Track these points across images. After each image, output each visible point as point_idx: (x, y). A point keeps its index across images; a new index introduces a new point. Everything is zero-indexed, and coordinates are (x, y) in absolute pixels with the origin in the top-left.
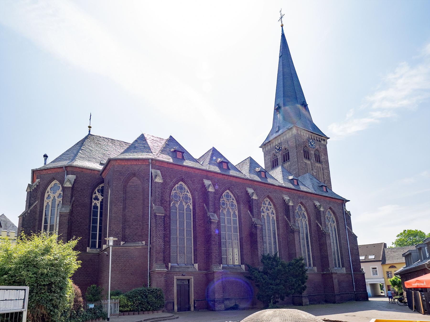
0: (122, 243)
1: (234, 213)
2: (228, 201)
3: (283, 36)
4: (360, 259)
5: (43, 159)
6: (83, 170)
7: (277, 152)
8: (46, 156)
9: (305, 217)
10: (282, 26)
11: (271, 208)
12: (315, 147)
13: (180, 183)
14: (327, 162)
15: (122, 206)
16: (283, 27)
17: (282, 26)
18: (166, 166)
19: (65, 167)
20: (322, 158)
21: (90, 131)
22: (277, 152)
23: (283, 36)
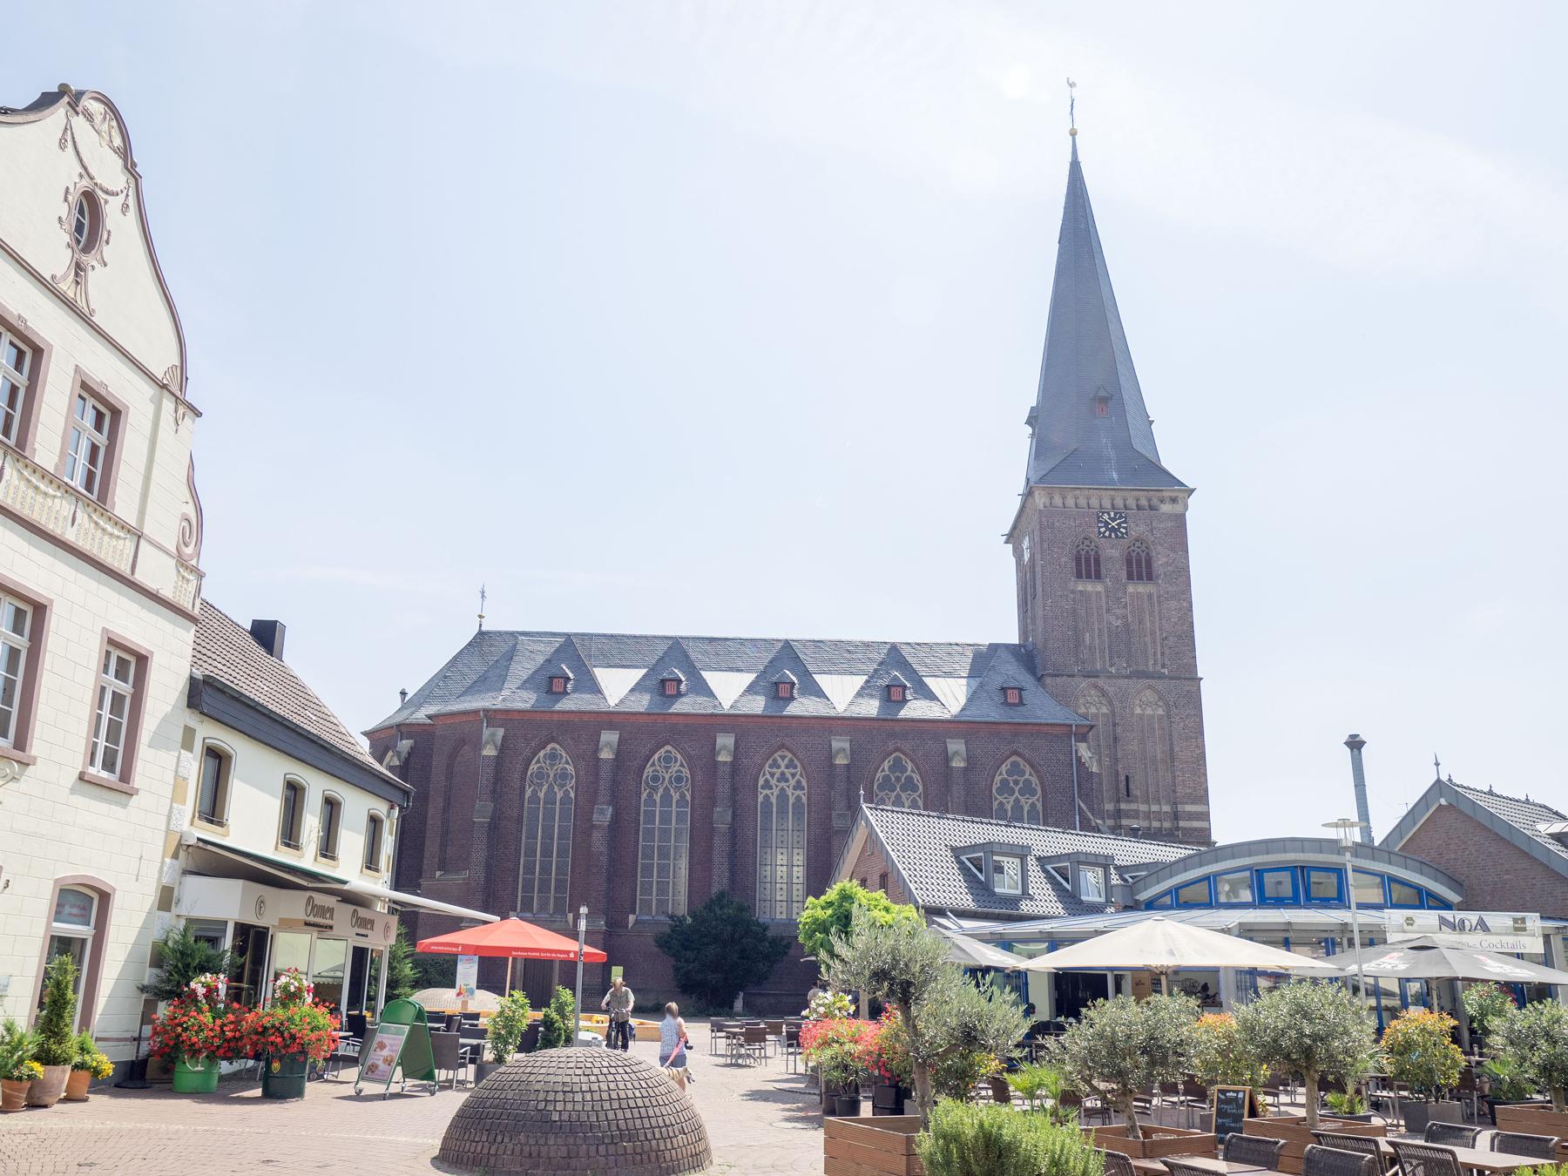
0: (438, 874)
1: (683, 796)
2: (667, 772)
3: (1075, 167)
4: (1266, 896)
5: (399, 697)
6: (426, 728)
7: (1124, 531)
8: (403, 694)
9: (914, 788)
10: (1073, 134)
11: (793, 775)
12: (1126, 533)
13: (549, 747)
14: (1182, 574)
15: (442, 805)
16: (1077, 137)
17: (1073, 134)
18: (516, 716)
19: (397, 726)
20: (1160, 562)
21: (480, 625)
22: (1124, 531)
23: (1075, 167)
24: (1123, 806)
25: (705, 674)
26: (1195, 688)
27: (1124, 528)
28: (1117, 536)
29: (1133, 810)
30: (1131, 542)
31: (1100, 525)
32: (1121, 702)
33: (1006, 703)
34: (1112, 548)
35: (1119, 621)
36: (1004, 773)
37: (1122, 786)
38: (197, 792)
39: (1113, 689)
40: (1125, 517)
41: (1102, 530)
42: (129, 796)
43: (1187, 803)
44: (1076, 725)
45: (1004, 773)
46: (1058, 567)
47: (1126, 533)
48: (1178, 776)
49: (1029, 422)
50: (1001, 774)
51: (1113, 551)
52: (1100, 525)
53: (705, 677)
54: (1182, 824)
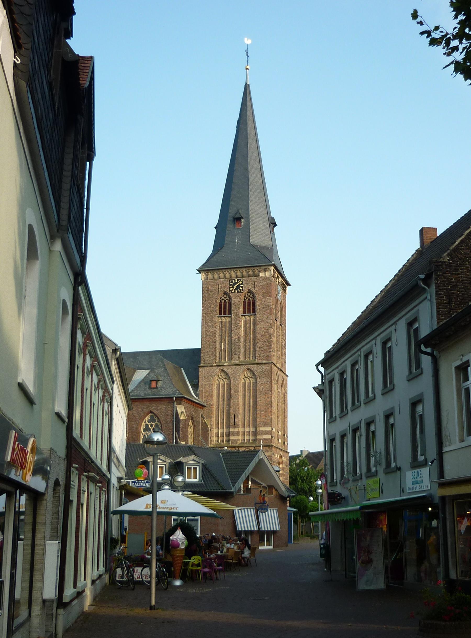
12: (242, 290)
24: (232, 430)
25: (438, 235)
26: (269, 368)
27: (242, 287)
28: (238, 292)
29: (236, 432)
30: (245, 294)
31: (230, 286)
32: (234, 377)
33: (150, 388)
34: (235, 298)
35: (236, 336)
36: (147, 422)
37: (232, 420)
38: (31, 175)
39: (230, 371)
40: (242, 281)
41: (231, 289)
42: (268, 545)
43: (261, 426)
44: (175, 398)
45: (147, 422)
46: (209, 311)
47: (242, 290)
48: (258, 413)
49: (215, 228)
50: (145, 422)
51: (236, 300)
52: (230, 286)
53: (440, 234)
54: (258, 437)
